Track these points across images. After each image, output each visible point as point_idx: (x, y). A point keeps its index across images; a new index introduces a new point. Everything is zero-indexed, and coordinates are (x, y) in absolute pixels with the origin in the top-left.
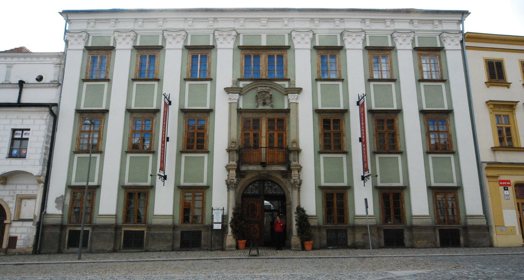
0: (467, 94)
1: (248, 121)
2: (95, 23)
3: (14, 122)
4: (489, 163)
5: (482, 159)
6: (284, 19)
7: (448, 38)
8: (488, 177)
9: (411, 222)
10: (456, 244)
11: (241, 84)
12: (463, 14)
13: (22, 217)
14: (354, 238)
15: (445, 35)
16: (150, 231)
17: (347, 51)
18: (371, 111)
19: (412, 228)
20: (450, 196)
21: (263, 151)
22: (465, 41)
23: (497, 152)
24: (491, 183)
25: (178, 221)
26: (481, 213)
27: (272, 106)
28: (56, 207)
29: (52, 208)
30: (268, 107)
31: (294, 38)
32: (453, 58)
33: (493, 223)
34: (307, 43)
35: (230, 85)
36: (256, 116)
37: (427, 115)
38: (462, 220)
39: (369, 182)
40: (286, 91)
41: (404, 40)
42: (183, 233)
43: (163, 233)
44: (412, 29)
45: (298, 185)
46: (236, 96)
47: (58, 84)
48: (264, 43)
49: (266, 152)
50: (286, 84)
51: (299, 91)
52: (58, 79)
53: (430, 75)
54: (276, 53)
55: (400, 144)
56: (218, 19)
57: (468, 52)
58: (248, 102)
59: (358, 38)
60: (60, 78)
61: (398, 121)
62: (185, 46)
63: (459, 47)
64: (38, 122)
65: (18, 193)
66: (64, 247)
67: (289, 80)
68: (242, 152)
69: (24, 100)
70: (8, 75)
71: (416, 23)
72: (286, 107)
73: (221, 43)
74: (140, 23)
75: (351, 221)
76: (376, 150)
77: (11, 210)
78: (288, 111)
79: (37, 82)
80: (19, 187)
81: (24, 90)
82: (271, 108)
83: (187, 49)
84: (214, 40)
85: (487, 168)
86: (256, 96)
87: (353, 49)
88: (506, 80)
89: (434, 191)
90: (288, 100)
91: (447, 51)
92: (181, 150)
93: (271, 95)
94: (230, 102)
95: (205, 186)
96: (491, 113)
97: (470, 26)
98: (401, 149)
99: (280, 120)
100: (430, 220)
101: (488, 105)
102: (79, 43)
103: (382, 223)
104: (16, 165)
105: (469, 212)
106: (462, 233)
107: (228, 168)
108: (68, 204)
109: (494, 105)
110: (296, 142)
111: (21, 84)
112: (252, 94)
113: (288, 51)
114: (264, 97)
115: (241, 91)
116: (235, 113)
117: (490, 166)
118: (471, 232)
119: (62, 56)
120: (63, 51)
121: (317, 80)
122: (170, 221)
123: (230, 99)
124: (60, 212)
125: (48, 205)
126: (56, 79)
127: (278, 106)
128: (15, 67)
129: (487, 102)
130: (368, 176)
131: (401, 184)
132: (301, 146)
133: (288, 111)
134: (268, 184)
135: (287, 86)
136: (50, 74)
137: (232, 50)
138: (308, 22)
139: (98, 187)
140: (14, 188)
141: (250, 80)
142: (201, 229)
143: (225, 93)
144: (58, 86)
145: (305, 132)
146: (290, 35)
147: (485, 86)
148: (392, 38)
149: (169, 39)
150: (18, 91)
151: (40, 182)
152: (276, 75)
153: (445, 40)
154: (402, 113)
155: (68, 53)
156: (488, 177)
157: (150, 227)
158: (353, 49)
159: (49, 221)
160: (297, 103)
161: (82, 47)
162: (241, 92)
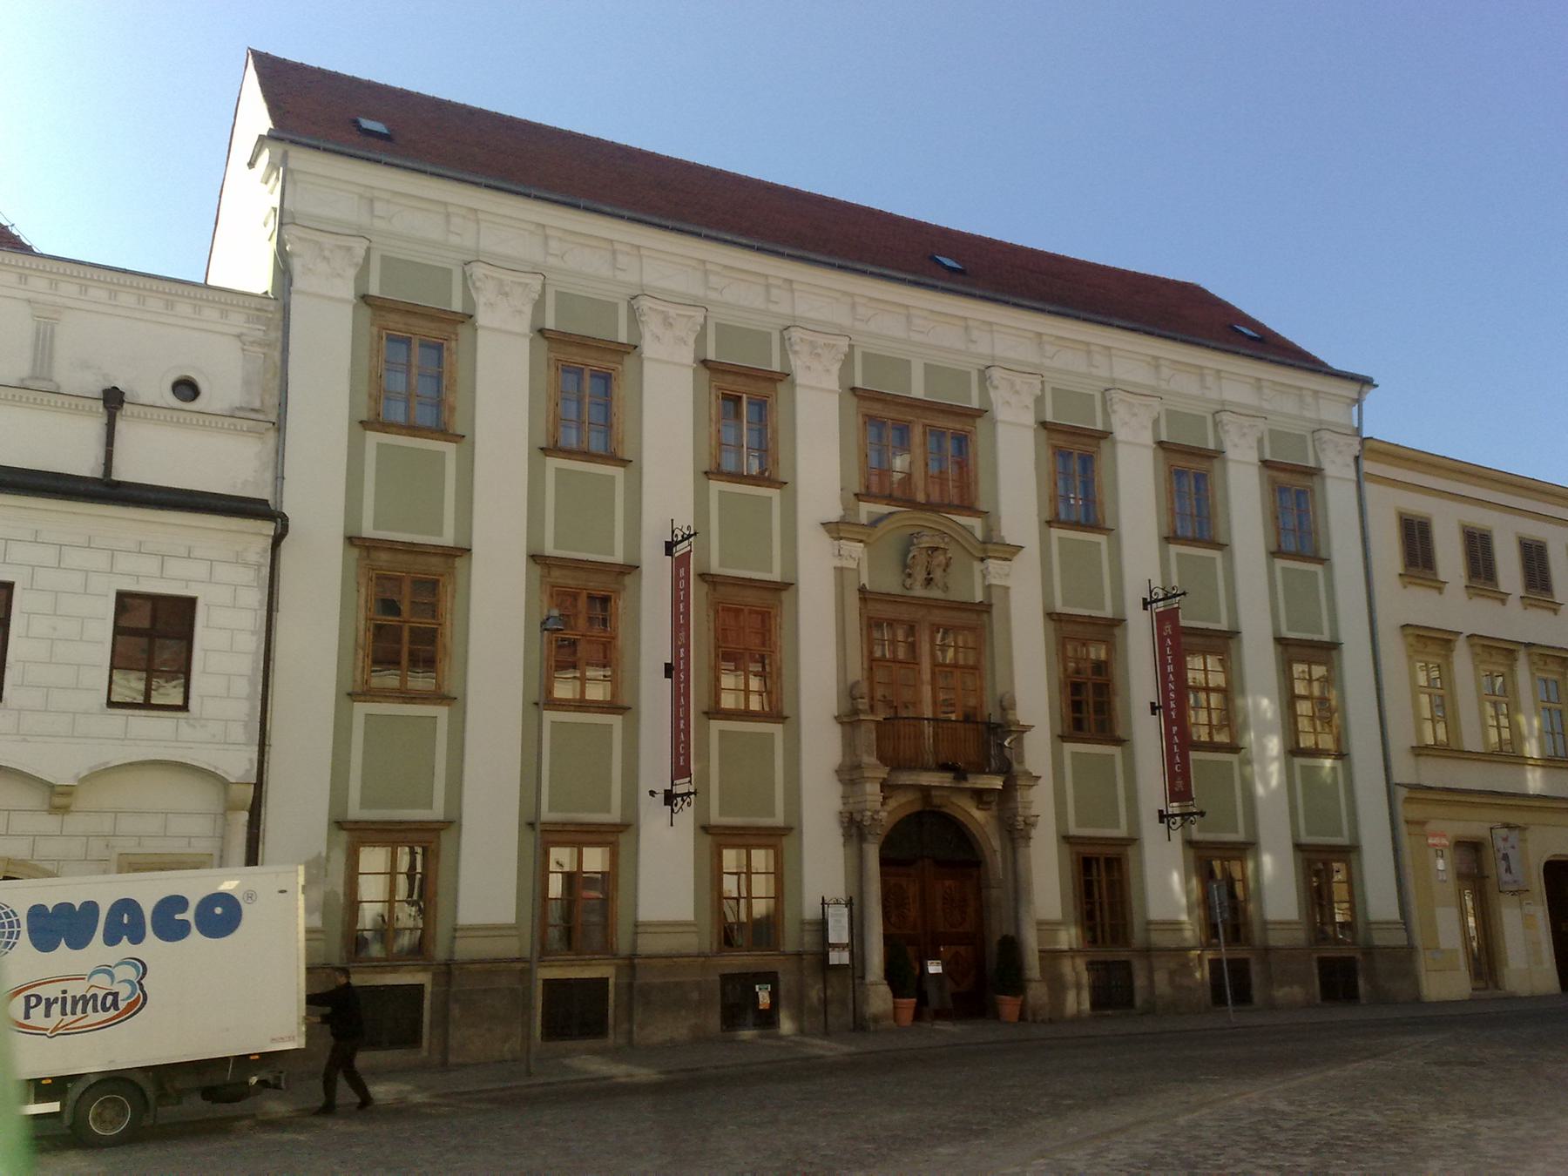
5: (1398, 777)
8: (1407, 822)
9: (634, 944)
11: (867, 510)
15: (1326, 436)
18: (703, 576)
27: (946, 588)
30: (935, 593)
31: (477, 289)
32: (1338, 497)
33: (1418, 941)
34: (520, 312)
35: (834, 513)
36: (905, 613)
39: (686, 816)
48: (918, 391)
54: (594, 361)
57: (1370, 489)
63: (1353, 475)
68: (881, 722)
69: (127, 471)
71: (1166, 372)
72: (979, 597)
75: (1138, 938)
78: (985, 608)
85: (1408, 800)
87: (667, 362)
88: (1436, 574)
92: (706, 709)
95: (615, 825)
97: (1383, 420)
98: (1120, 733)
104: (152, 734)
116: (853, 600)
117: (1419, 795)
121: (1049, 523)
122: (689, 943)
126: (257, 405)
129: (1404, 627)
130: (689, 794)
131: (1122, 832)
132: (1022, 715)
133: (985, 608)
139: (450, 824)
143: (825, 539)
147: (1397, 580)
157: (631, 963)
158: (667, 362)
160: (1007, 589)
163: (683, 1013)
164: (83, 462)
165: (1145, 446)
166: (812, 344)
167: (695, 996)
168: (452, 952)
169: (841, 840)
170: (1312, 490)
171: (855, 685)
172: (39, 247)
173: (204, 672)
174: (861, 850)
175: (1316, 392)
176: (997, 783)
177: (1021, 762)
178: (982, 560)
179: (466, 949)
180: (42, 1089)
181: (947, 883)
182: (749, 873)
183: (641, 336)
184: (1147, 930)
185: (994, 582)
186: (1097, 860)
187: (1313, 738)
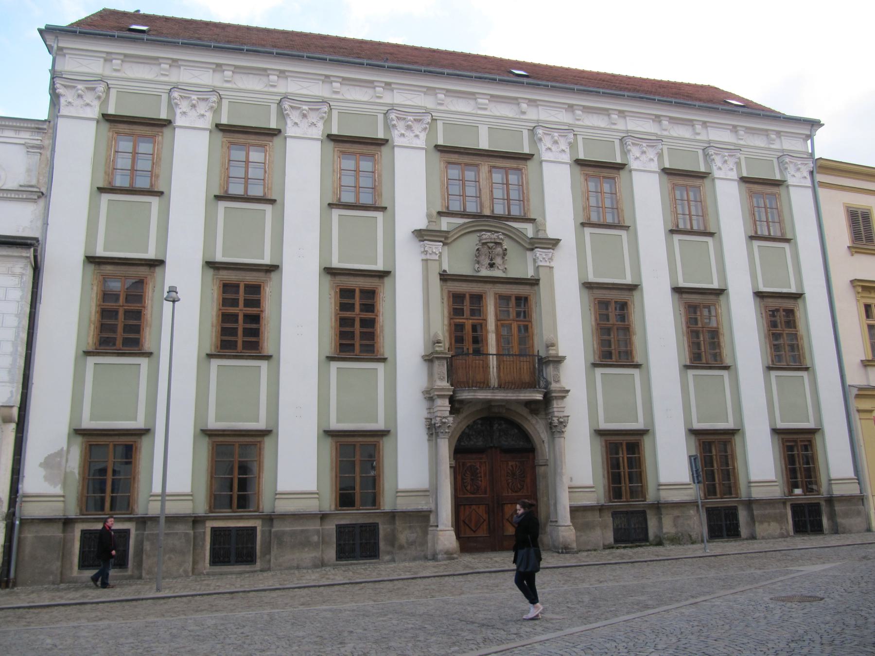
0: (820, 265)
1: (462, 301)
2: (123, 61)
4: (860, 389)
5: (849, 381)
6: (520, 100)
7: (791, 165)
8: (858, 411)
9: (749, 493)
10: (817, 529)
11: (445, 224)
12: (813, 125)
14: (660, 527)
15: (787, 160)
16: (272, 526)
17: (396, 149)
19: (750, 504)
20: (29, 535)
21: (493, 361)
22: (818, 173)
23: (869, 369)
24: (863, 421)
25: (327, 502)
26: (851, 474)
27: (505, 270)
28: (46, 478)
29: (34, 481)
30: (497, 273)
32: (799, 199)
34: (563, 151)
35: (422, 224)
36: (475, 288)
37: (766, 300)
38: (824, 489)
40: (530, 243)
41: (725, 162)
42: (340, 529)
43: (302, 531)
44: (659, 133)
45: (556, 429)
46: (437, 247)
47: (37, 194)
48: (484, 144)
49: (498, 361)
50: (529, 230)
51: (554, 243)
52: (38, 181)
53: (616, 217)
55: (726, 351)
56: (393, 86)
57: (822, 192)
58: (459, 259)
59: (650, 149)
60: (43, 180)
61: (268, 291)
62: (104, 115)
63: (809, 184)
66: (71, 568)
67: (532, 221)
72: (530, 273)
73: (403, 135)
74: (228, 74)
75: (651, 496)
76: (688, 363)
78: (534, 282)
82: (503, 275)
83: (107, 120)
84: (171, 107)
85: (858, 396)
86: (478, 250)
89: (92, 440)
90: (535, 261)
91: (791, 188)
93: (506, 250)
94: (424, 257)
96: (858, 301)
97: (825, 146)
98: (728, 361)
99: (522, 300)
100: (777, 488)
101: (854, 287)
102: (88, 105)
103: (333, 507)
105: (664, 478)
106: (824, 508)
107: (430, 396)
108: (76, 471)
109: (864, 288)
110: (551, 345)
112: (470, 243)
113: (622, 172)
114: (489, 251)
115: (446, 238)
118: (838, 508)
119: (45, 129)
120: (44, 117)
122: (311, 506)
123: (425, 252)
124: (58, 490)
126: (34, 182)
127: (514, 272)
129: (852, 282)
132: (562, 350)
133: (534, 282)
134: (500, 425)
135: (530, 234)
138: (321, 82)
141: (463, 215)
142: (377, 520)
144: (39, 197)
145: (567, 326)
146: (532, 131)
148: (706, 155)
149: (635, 151)
151: (7, 420)
152: (515, 211)
153: (786, 169)
154: (728, 295)
156: (858, 411)
159: (31, 510)
161: (94, 112)
162: (444, 238)
163: (306, 550)
165: (566, 163)
166: (795, 165)
167: (315, 538)
168: (147, 509)
169: (426, 437)
170: (780, 195)
174: (436, 443)
175: (704, 123)
176: (539, 397)
177: (558, 381)
178: (532, 249)
179: (284, 506)
181: (510, 463)
183: (175, 114)
184: (830, 485)
185: (541, 264)
186: (621, 444)
187: (495, 352)
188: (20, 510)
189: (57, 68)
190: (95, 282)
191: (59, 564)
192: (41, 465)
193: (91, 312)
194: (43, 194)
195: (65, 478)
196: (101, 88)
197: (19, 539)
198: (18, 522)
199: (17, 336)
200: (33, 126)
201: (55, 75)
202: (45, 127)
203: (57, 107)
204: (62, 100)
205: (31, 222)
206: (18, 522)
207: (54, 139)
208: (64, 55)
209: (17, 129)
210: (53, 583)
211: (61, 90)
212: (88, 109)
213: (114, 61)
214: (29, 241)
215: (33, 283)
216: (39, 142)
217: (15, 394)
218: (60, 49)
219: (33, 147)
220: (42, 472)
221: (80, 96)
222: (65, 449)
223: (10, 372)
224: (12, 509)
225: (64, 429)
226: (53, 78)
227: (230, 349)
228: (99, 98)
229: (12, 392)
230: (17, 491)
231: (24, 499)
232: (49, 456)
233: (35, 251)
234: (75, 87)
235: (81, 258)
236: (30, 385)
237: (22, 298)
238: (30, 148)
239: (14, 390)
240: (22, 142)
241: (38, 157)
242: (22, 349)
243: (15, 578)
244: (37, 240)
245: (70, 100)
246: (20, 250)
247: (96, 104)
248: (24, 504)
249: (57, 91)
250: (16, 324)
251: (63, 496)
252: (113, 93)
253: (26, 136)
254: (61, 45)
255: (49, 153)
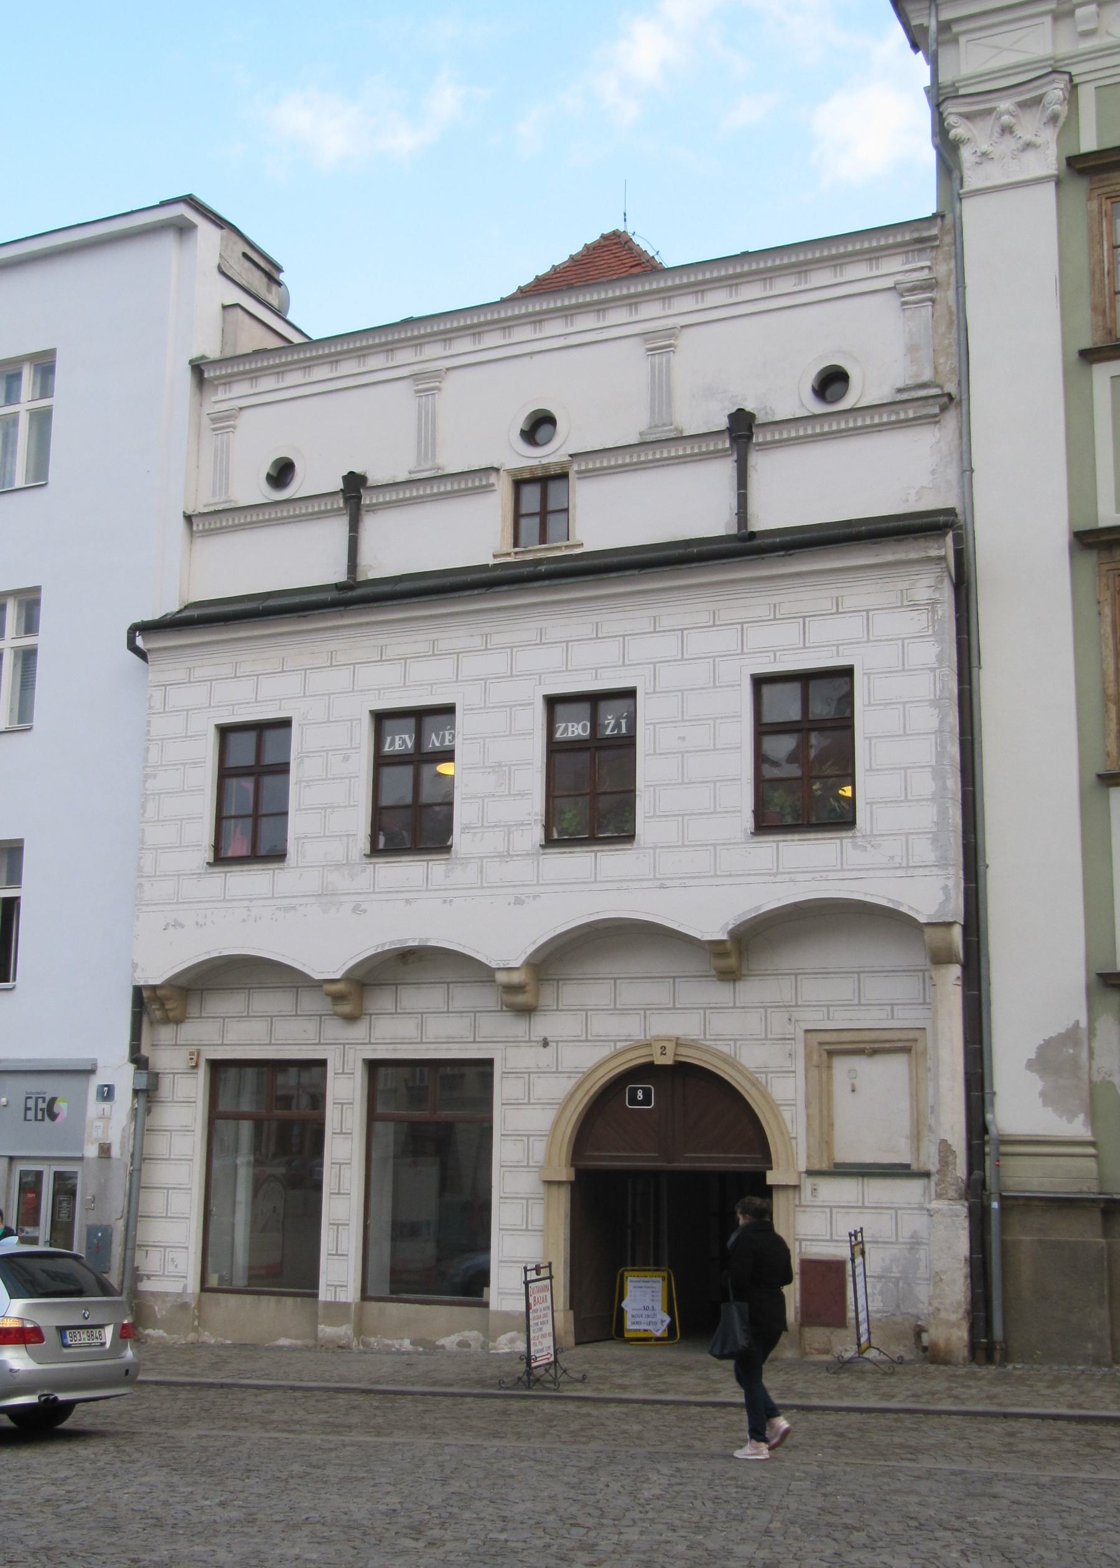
3: (758, 637)
13: (846, 1154)
20: (1026, 1236)
28: (1046, 1098)
29: (1022, 1106)
47: (941, 401)
60: (947, 364)
64: (888, 624)
65: (815, 1019)
69: (768, 517)
70: (661, 390)
77: (787, 1115)
79: (819, 408)
80: (812, 990)
81: (758, 462)
102: (1029, 146)
104: (808, 868)
111: (742, 429)
119: (933, 237)
120: (929, 208)
124: (1078, 1128)
125: (997, 1088)
126: (927, 376)
128: (687, 342)
136: (882, 348)
137: (1052, 186)
140: (787, 996)
144: (944, 409)
150: (726, 469)
151: (940, 958)
155: (971, 212)
159: (1026, 1176)
161: (1046, 161)
164: (715, 522)
171: (443, 469)
172: (669, 259)
173: (871, 770)
180: (596, 1314)
182: (256, 816)
188: (998, 1177)
189: (945, 78)
190: (1107, 595)
191: (1104, 1314)
192: (1030, 1065)
193: (1104, 674)
194: (949, 396)
195: (1092, 1096)
196: (1056, 91)
197: (1003, 1244)
198: (995, 1205)
199: (941, 754)
200: (908, 237)
201: (940, 97)
202: (935, 231)
203: (956, 174)
204: (966, 154)
205: (933, 472)
206: (995, 1205)
207: (959, 257)
208: (955, 40)
209: (872, 256)
210: (1097, 1362)
211: (959, 130)
212: (1030, 156)
213: (1079, 12)
214: (942, 519)
215: (958, 621)
216: (925, 274)
217: (952, 893)
218: (945, 27)
219: (913, 290)
220: (1035, 1083)
221: (1007, 130)
222: (1083, 1023)
223: (935, 840)
224: (977, 1173)
225: (1074, 976)
226: (937, 108)
227: (318, 1100)
228: (1054, 118)
229: (945, 888)
230: (985, 1130)
231: (1005, 1149)
232: (1048, 1043)
233: (959, 540)
234: (990, 112)
235: (1062, 539)
236: (981, 869)
237: (940, 659)
238: (906, 293)
239: (951, 883)
240: (889, 282)
241: (927, 311)
242: (954, 783)
243: (1005, 1341)
244: (951, 512)
245: (985, 147)
246: (922, 543)
247: (1048, 137)
248: (1004, 1161)
249: (952, 134)
250: (934, 724)
251: (1093, 1144)
252: (1087, 96)
253: (895, 268)
254: (946, 15)
255: (951, 295)
